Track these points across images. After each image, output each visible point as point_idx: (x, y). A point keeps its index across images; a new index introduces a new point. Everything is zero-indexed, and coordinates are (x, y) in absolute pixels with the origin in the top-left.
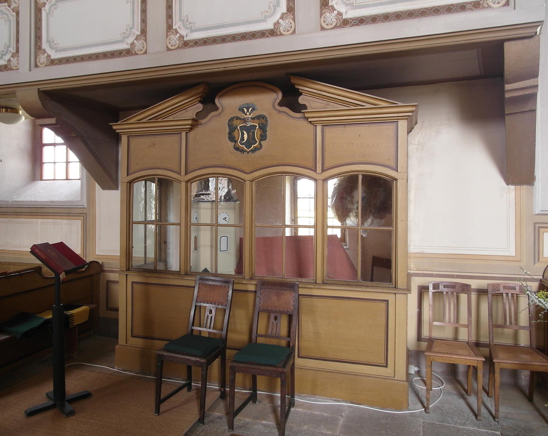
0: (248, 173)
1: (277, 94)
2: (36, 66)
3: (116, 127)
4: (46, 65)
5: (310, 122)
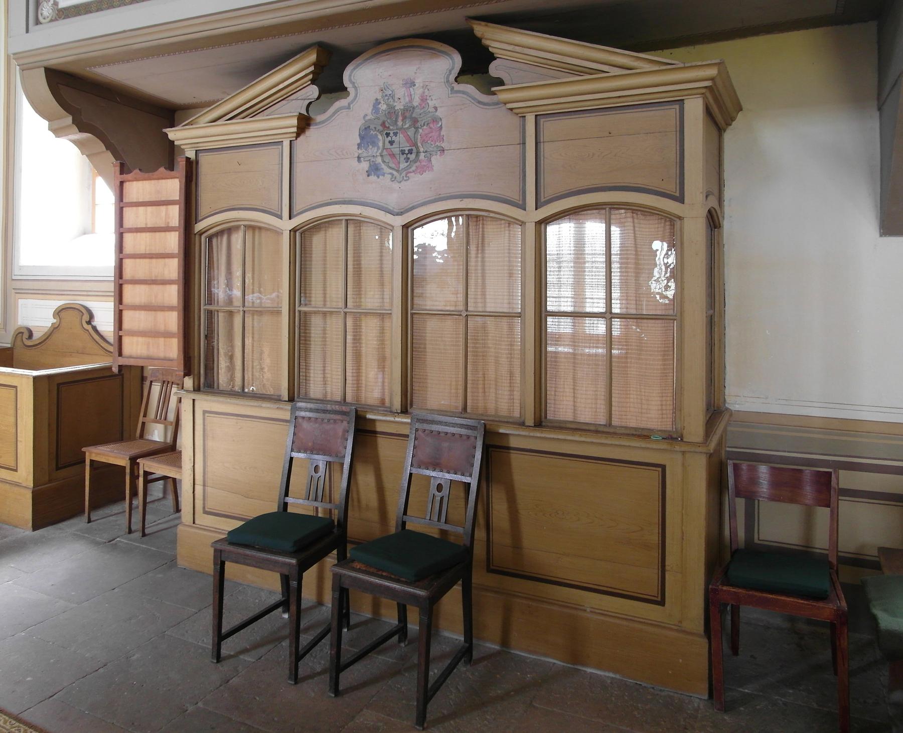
0: (398, 214)
1: (452, 59)
2: (37, 22)
3: (173, 134)
4: (51, 21)
5: (511, 109)
